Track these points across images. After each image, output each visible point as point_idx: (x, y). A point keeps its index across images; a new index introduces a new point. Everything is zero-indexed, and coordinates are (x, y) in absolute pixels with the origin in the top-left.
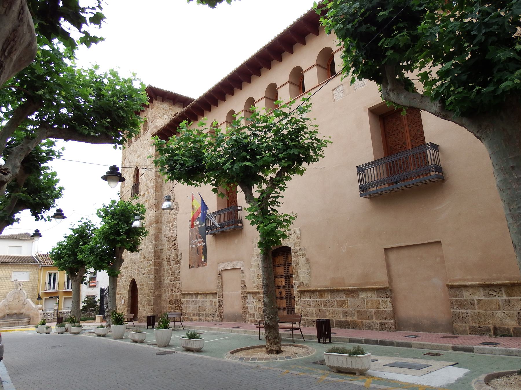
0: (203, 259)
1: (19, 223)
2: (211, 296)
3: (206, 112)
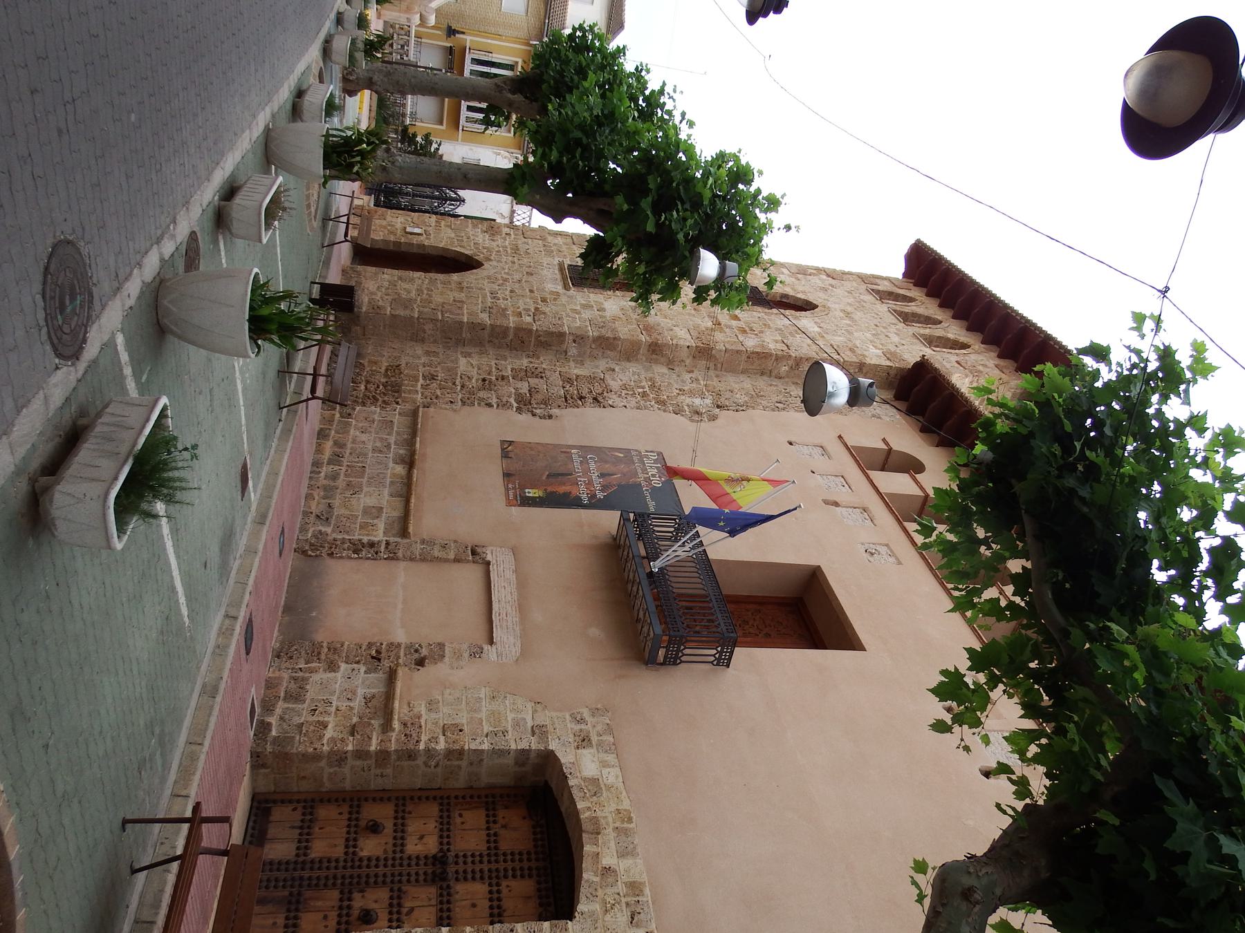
0: (531, 493)
2: (396, 514)
3: (902, 405)
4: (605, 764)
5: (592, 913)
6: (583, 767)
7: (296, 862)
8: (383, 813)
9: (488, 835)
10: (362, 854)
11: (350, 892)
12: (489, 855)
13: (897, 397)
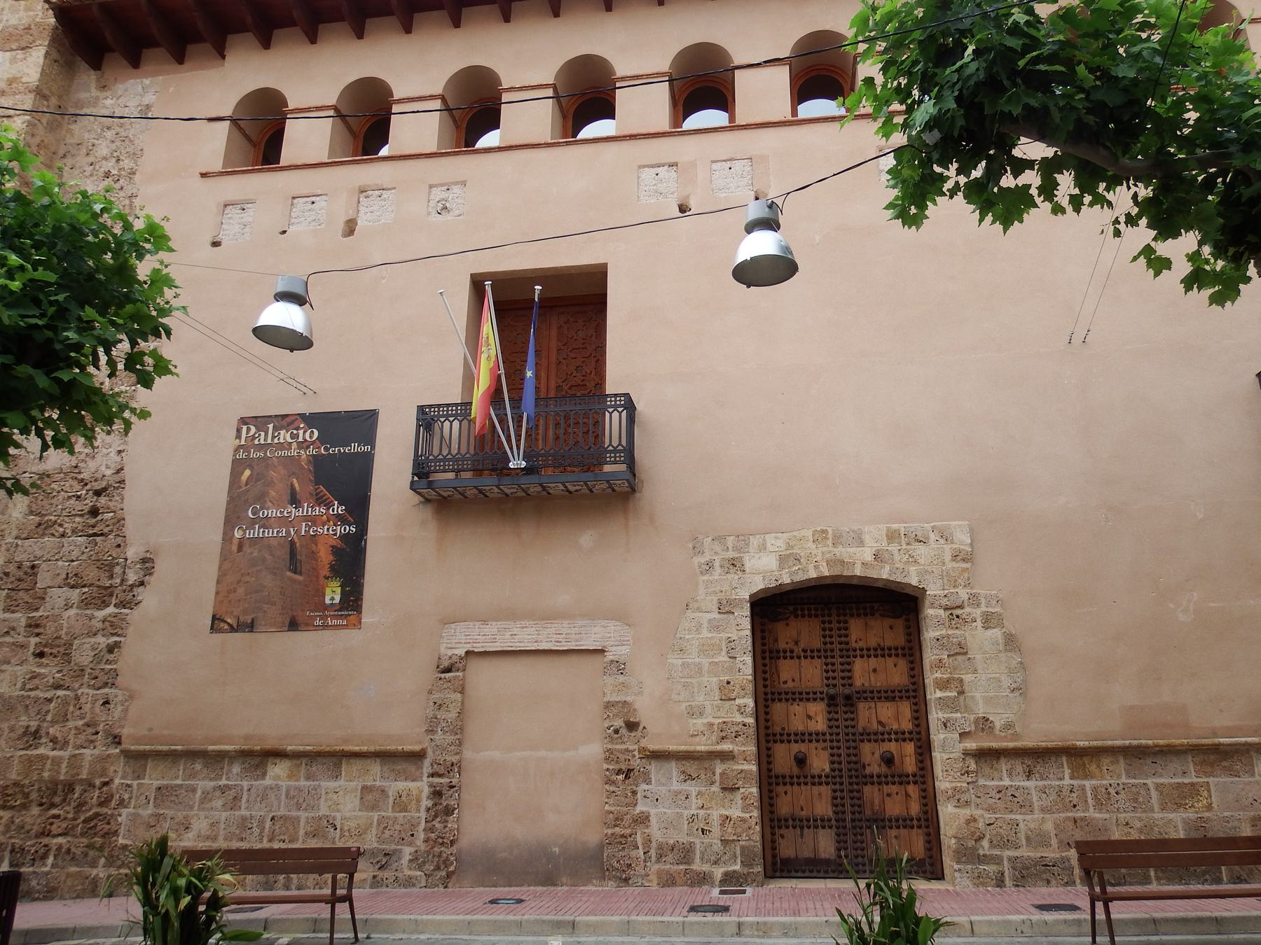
2: (376, 768)
3: (114, 63)
4: (763, 548)
5: (919, 573)
6: (766, 569)
7: (838, 828)
8: (783, 757)
9: (806, 657)
10: (828, 770)
11: (865, 777)
12: (826, 657)
13: (96, 65)
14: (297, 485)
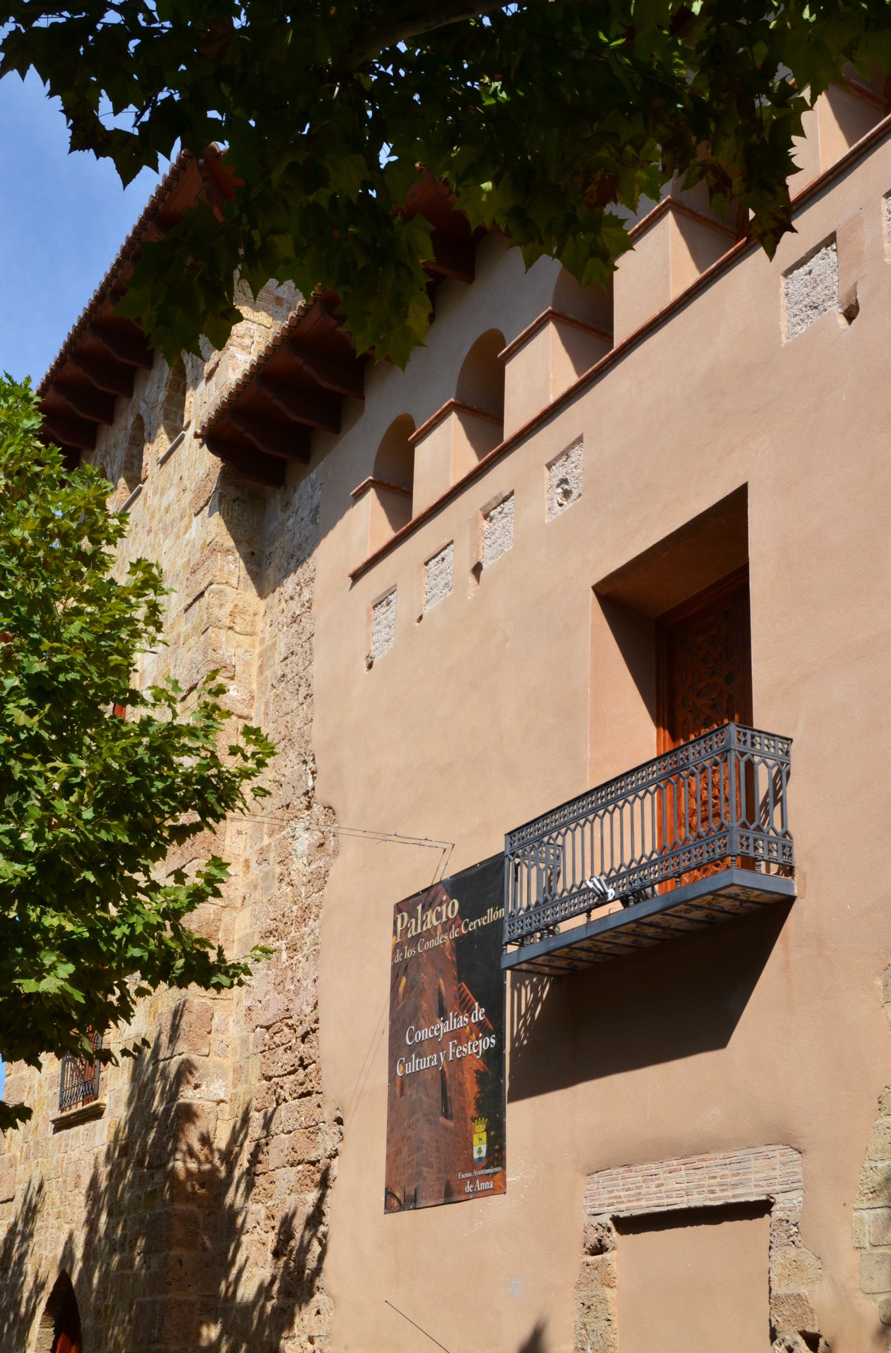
0: (480, 1148)
1: (793, 230)
14: (443, 988)
